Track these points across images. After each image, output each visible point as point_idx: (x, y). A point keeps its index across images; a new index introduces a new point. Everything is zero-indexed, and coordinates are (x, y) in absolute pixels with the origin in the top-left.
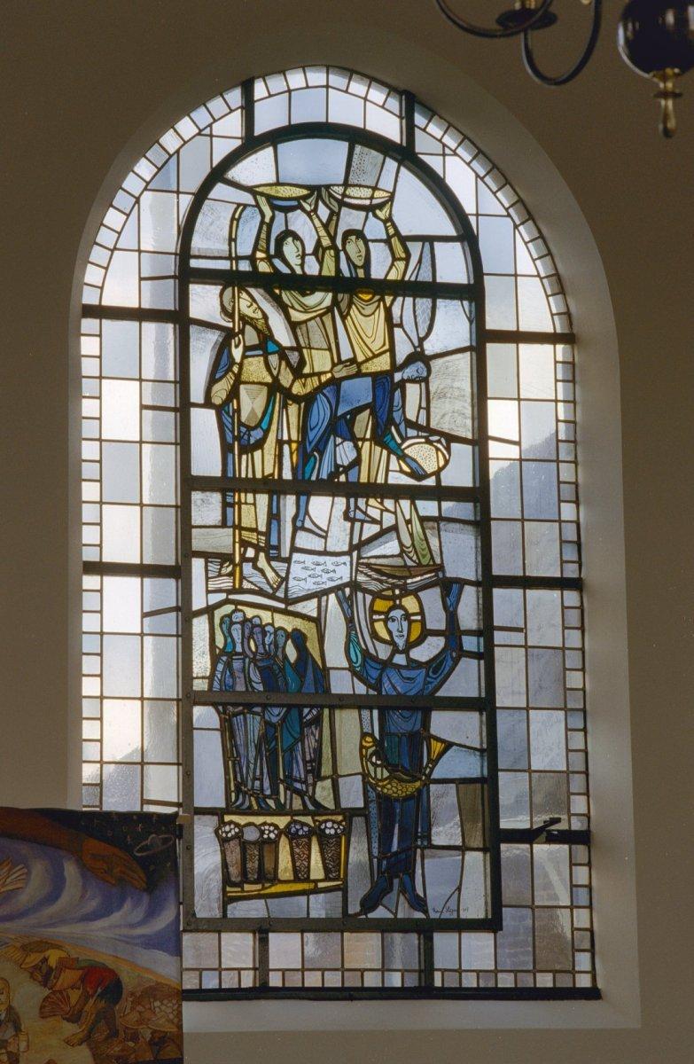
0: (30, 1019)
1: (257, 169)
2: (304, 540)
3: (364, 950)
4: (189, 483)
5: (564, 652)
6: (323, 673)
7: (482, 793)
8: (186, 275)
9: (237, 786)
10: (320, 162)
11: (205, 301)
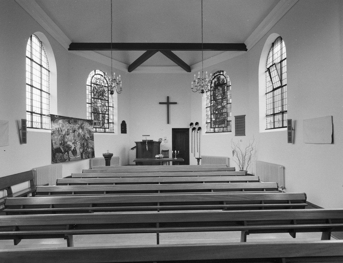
0: (87, 134)
1: (95, 76)
2: (98, 102)
3: (101, 129)
4: (92, 98)
5: (32, 115)
6: (99, 111)
7: (108, 120)
8: (92, 83)
9: (94, 119)
10: (99, 76)
11: (93, 85)
